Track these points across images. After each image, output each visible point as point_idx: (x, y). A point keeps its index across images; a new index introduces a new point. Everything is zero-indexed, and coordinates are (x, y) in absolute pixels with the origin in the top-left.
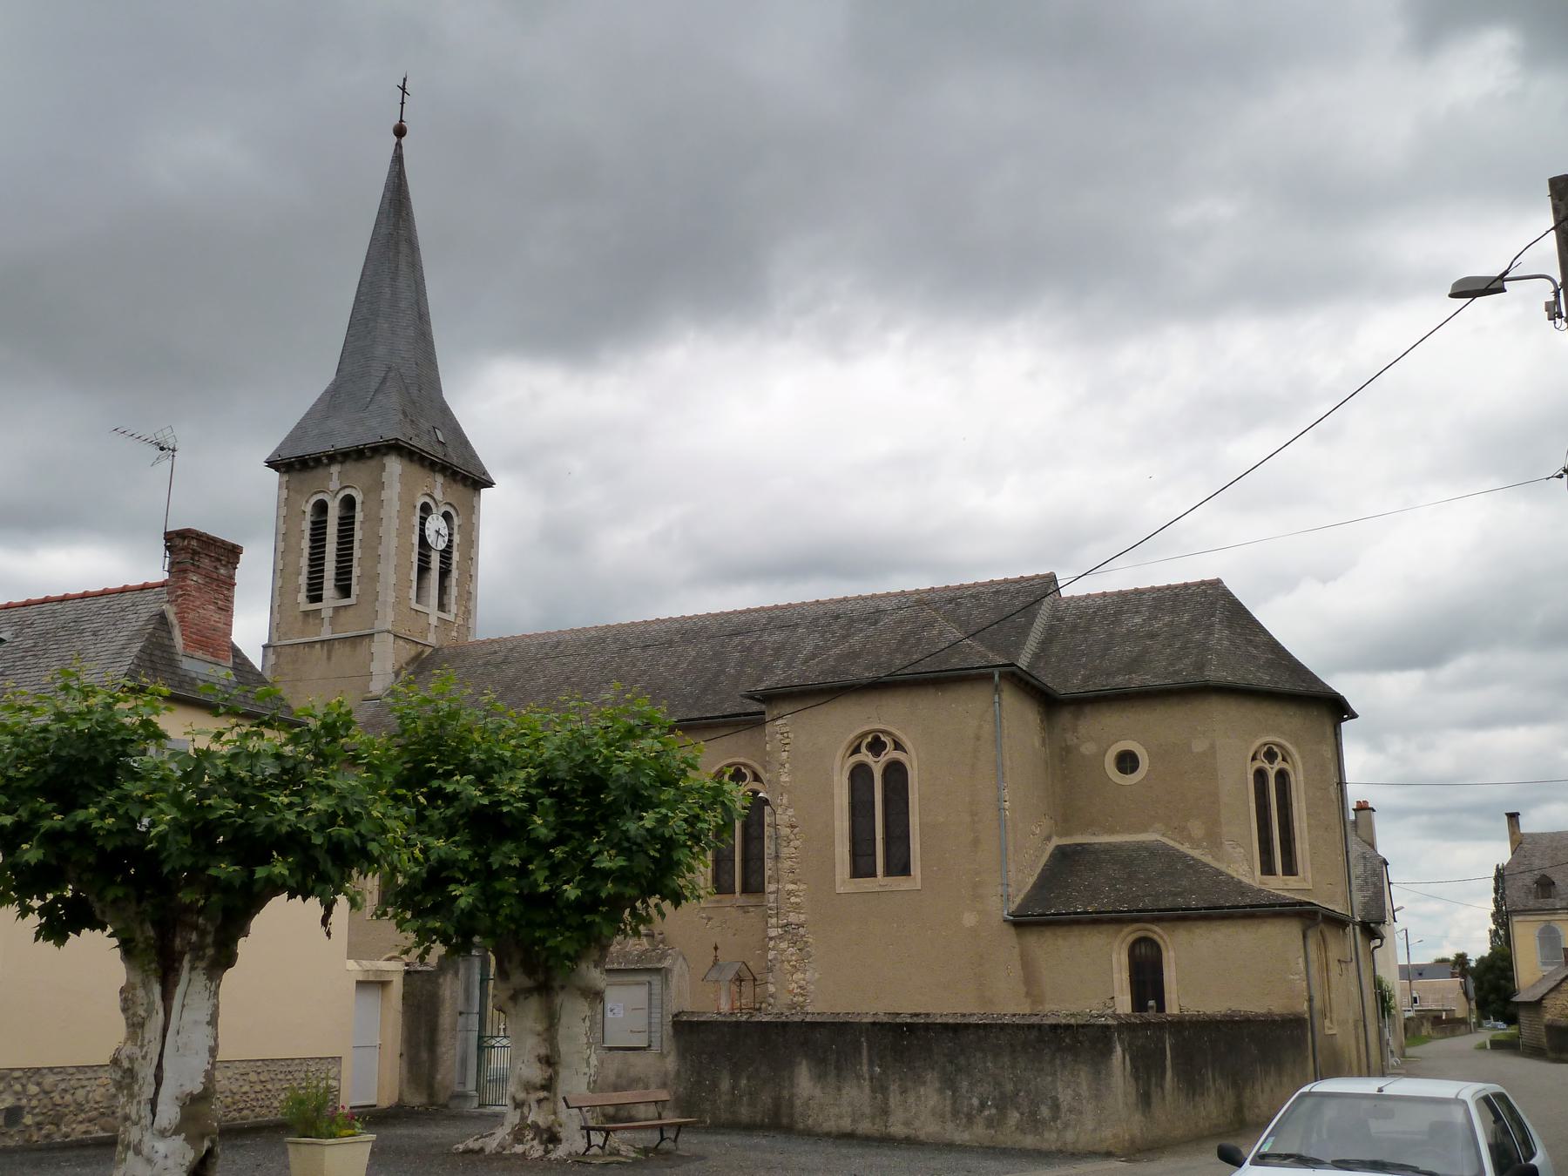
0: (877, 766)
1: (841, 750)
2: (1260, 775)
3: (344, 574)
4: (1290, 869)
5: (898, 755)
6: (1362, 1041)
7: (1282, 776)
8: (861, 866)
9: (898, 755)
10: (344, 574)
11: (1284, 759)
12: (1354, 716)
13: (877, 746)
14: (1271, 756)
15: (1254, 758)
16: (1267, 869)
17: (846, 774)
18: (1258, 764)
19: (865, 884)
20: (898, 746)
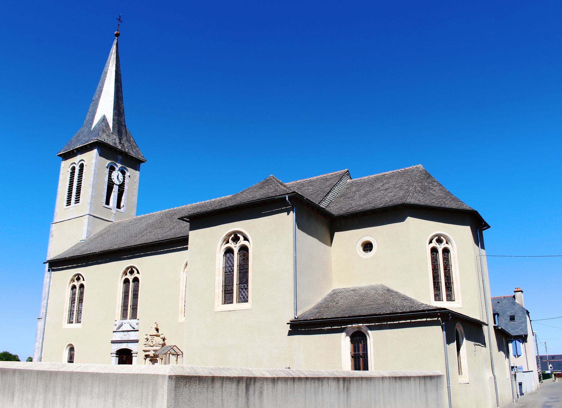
0: (236, 248)
1: (220, 242)
2: (434, 251)
3: (72, 174)
4: (450, 298)
5: (246, 243)
6: (483, 300)
7: (446, 251)
8: (228, 297)
9: (246, 243)
10: (72, 174)
11: (447, 243)
12: (290, 333)
13: (236, 239)
14: (439, 241)
15: (431, 242)
16: (438, 297)
17: (222, 253)
18: (432, 245)
19: (228, 307)
20: (246, 239)
